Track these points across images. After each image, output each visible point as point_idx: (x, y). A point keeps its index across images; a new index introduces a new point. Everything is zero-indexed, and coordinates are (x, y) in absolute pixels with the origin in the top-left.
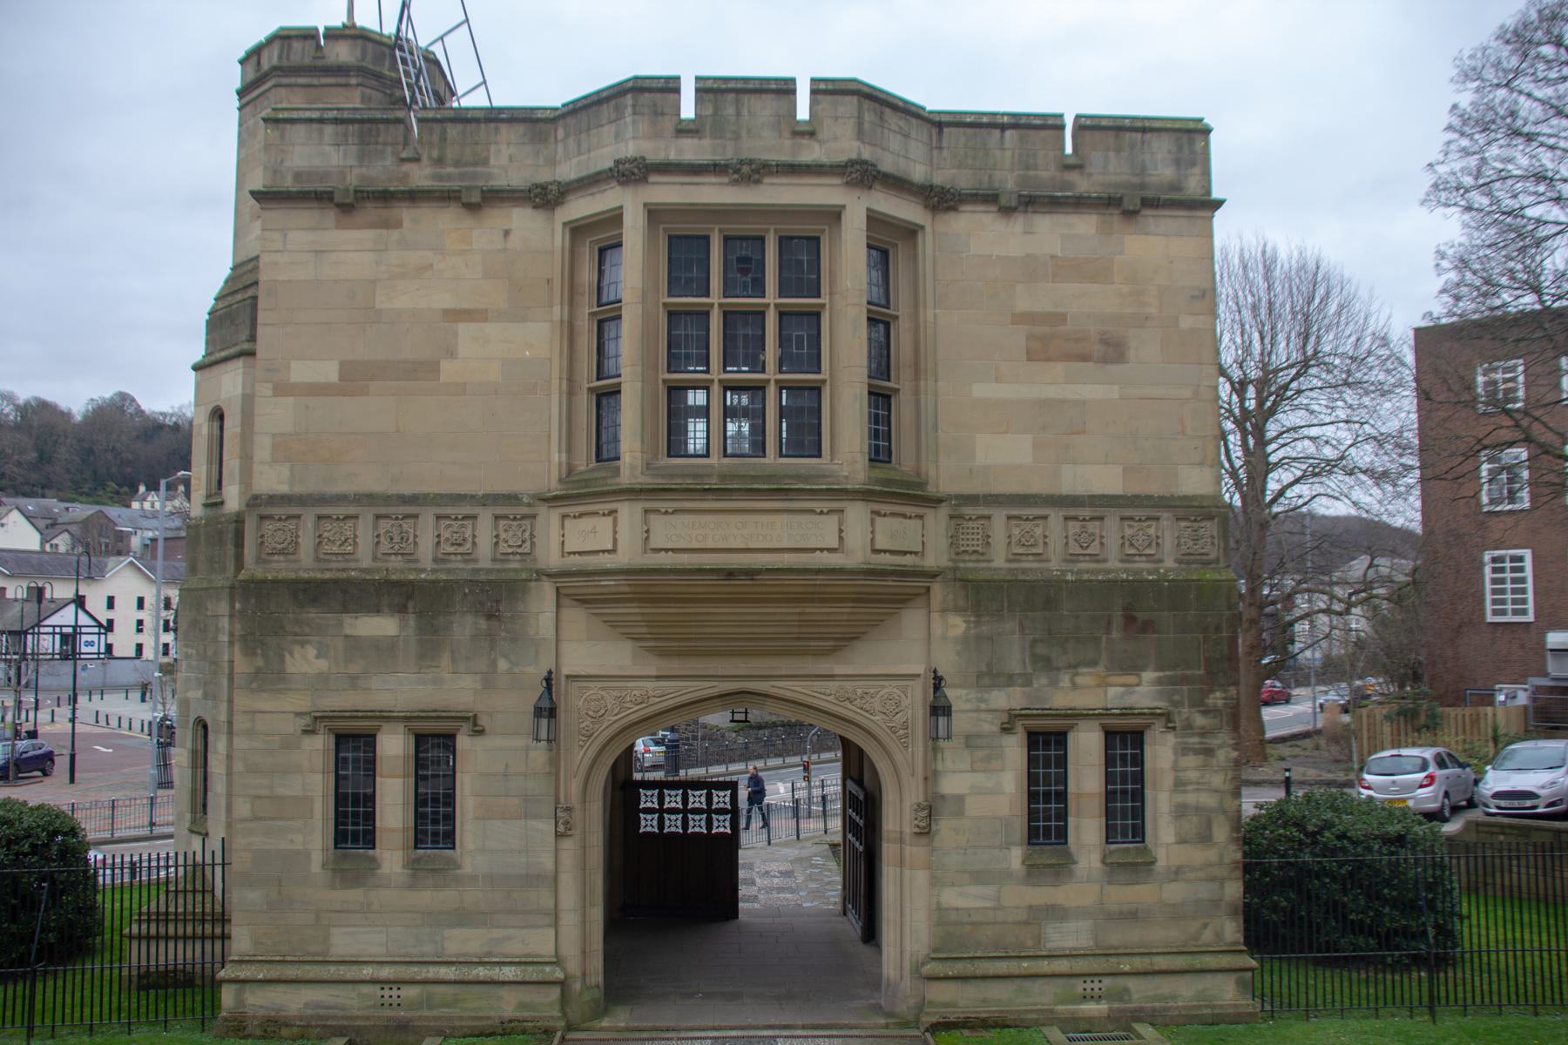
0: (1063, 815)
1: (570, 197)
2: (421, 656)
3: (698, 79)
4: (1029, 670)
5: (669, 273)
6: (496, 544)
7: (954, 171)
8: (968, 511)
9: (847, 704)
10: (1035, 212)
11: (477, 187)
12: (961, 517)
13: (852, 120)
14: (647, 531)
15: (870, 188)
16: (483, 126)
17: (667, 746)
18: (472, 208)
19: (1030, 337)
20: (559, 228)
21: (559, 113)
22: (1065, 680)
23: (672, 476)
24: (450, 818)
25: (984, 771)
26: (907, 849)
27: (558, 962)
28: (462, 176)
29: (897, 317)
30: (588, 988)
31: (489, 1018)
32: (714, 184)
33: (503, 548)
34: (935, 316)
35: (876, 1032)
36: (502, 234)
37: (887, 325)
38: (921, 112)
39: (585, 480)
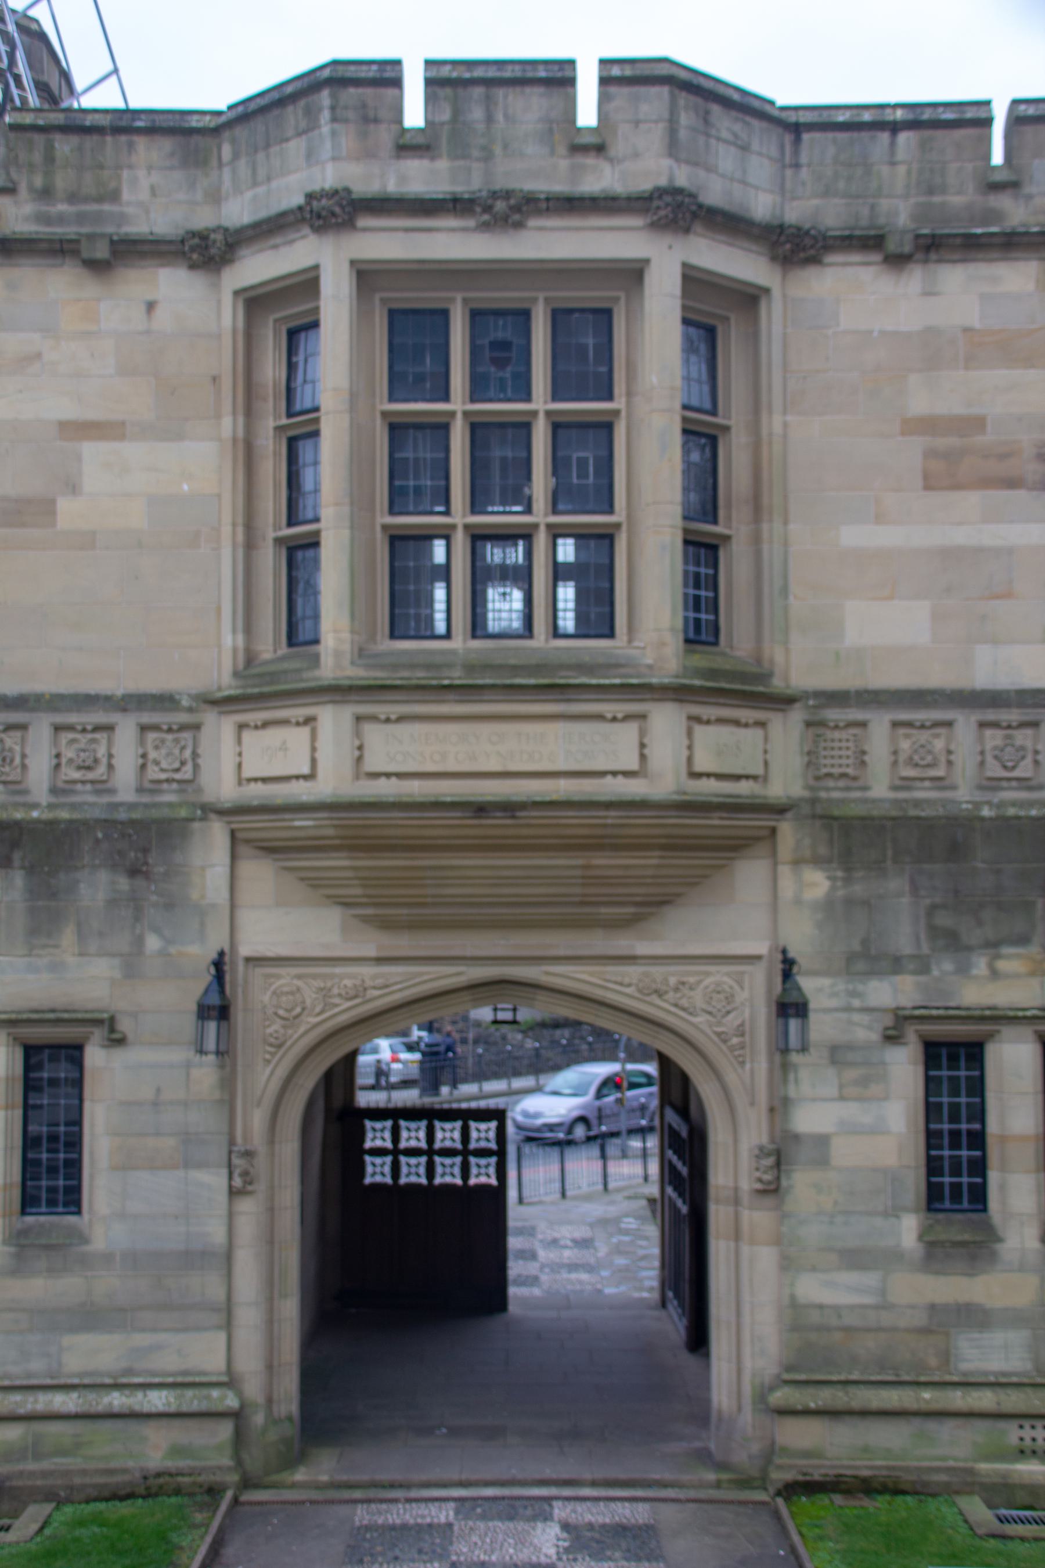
0: (979, 1167)
1: (243, 252)
2: (33, 932)
3: (429, 63)
4: (925, 949)
5: (391, 367)
6: (143, 767)
7: (815, 202)
8: (833, 714)
9: (654, 999)
10: (940, 261)
11: (103, 235)
12: (822, 724)
13: (661, 126)
14: (360, 748)
15: (687, 231)
16: (109, 139)
17: (424, 1054)
18: (98, 267)
19: (930, 454)
20: (227, 299)
21: (223, 119)
22: (980, 965)
23: (395, 667)
24: (74, 1167)
25: (859, 1099)
26: (746, 1214)
27: (231, 1381)
28: (81, 218)
29: (726, 429)
30: (276, 1422)
31: (125, 1471)
32: (453, 230)
33: (153, 773)
34: (785, 425)
35: (702, 1494)
36: (143, 308)
37: (713, 440)
38: (768, 108)
39: (272, 674)
